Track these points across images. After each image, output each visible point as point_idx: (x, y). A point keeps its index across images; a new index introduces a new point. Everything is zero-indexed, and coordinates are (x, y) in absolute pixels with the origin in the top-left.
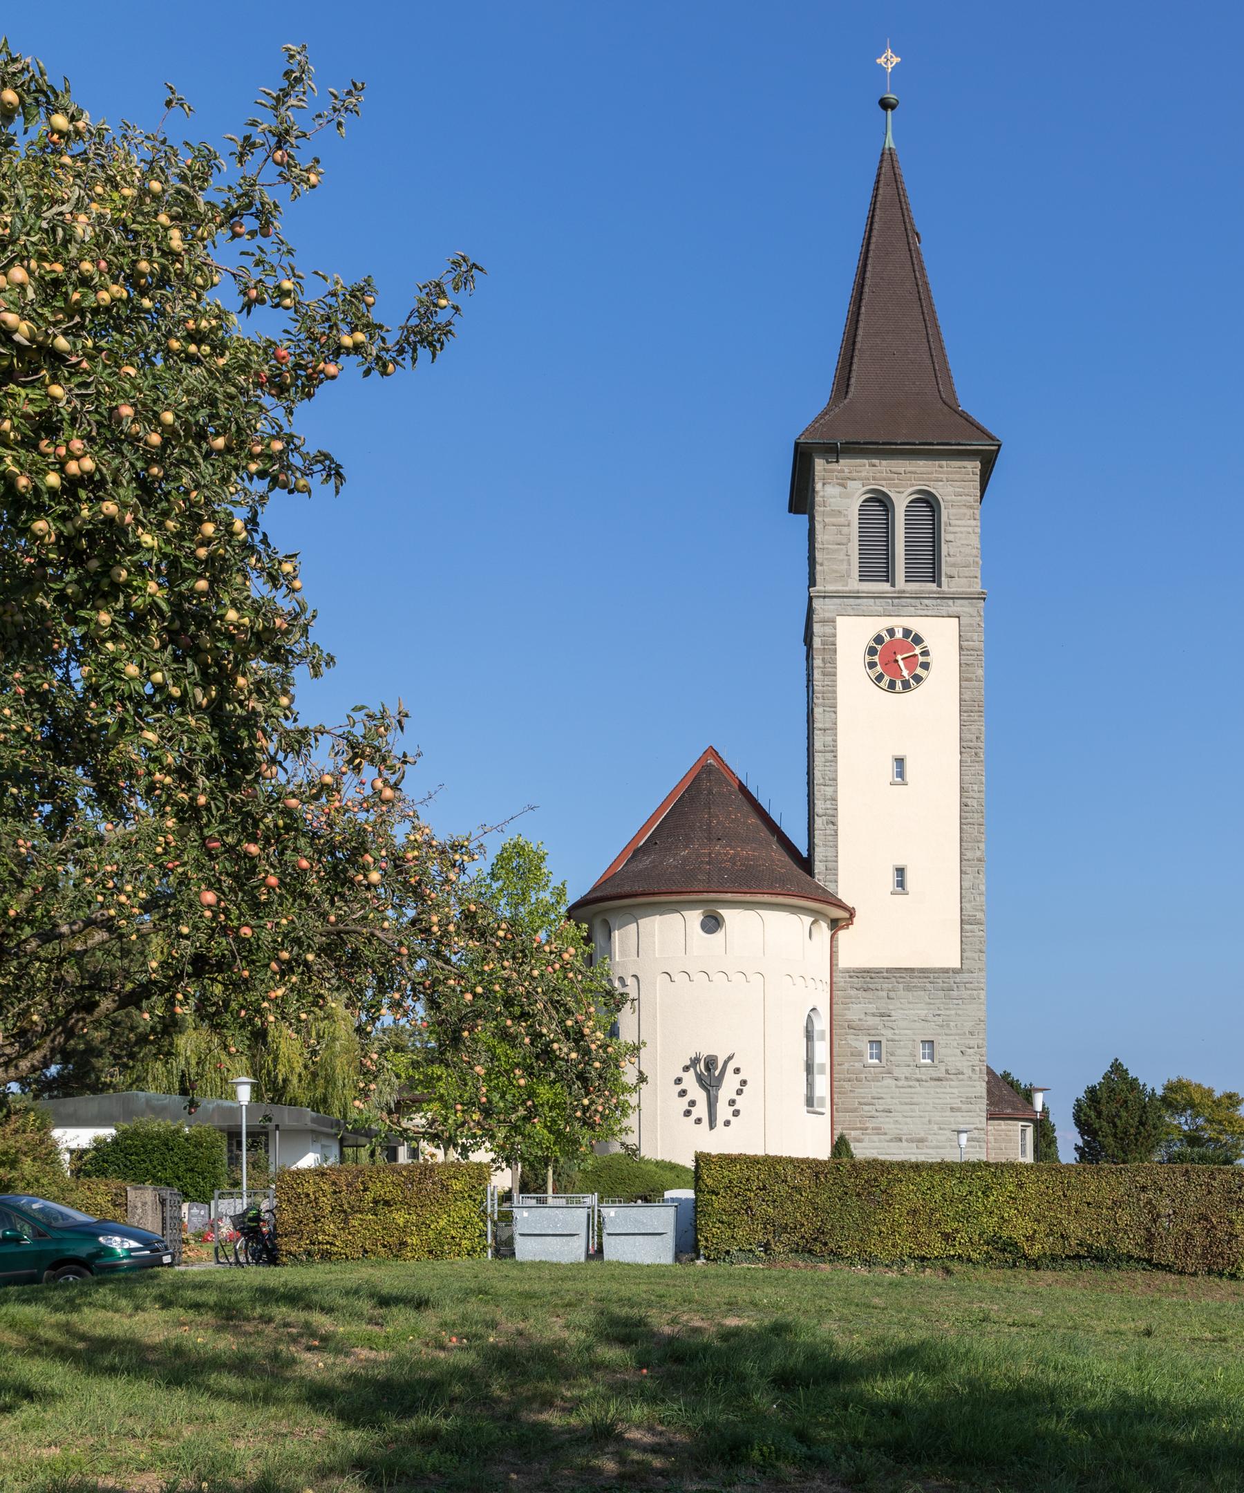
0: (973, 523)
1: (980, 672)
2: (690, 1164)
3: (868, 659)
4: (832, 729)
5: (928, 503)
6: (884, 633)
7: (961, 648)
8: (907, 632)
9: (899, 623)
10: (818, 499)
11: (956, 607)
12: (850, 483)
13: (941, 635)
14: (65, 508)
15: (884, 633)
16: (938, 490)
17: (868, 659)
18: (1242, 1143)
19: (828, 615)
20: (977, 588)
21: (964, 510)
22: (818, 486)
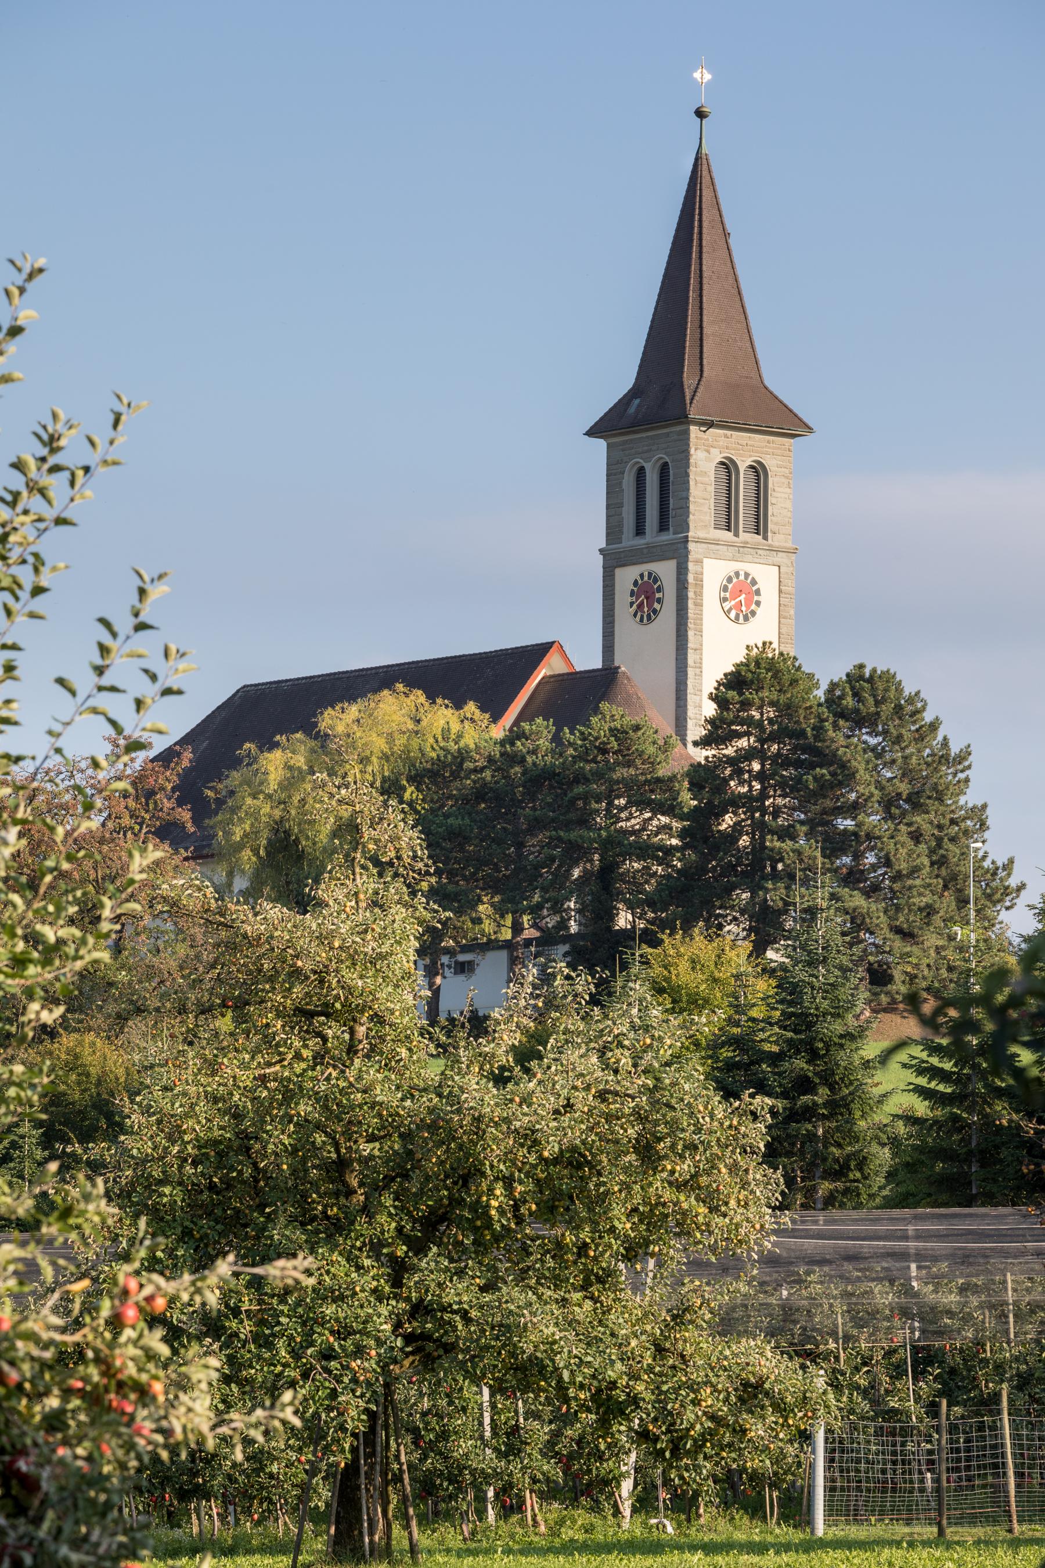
0: (788, 490)
1: (792, 612)
2: (844, 678)
3: (732, 574)
4: (699, 650)
5: (759, 471)
6: (742, 573)
7: (780, 591)
8: (747, 575)
9: (742, 567)
10: (692, 461)
11: (781, 558)
12: (712, 450)
13: (766, 577)
14: (161, 1399)
15: (742, 573)
16: (769, 463)
17: (732, 574)
18: (7, 1314)
19: (699, 556)
20: (790, 545)
21: (783, 480)
22: (692, 451)
